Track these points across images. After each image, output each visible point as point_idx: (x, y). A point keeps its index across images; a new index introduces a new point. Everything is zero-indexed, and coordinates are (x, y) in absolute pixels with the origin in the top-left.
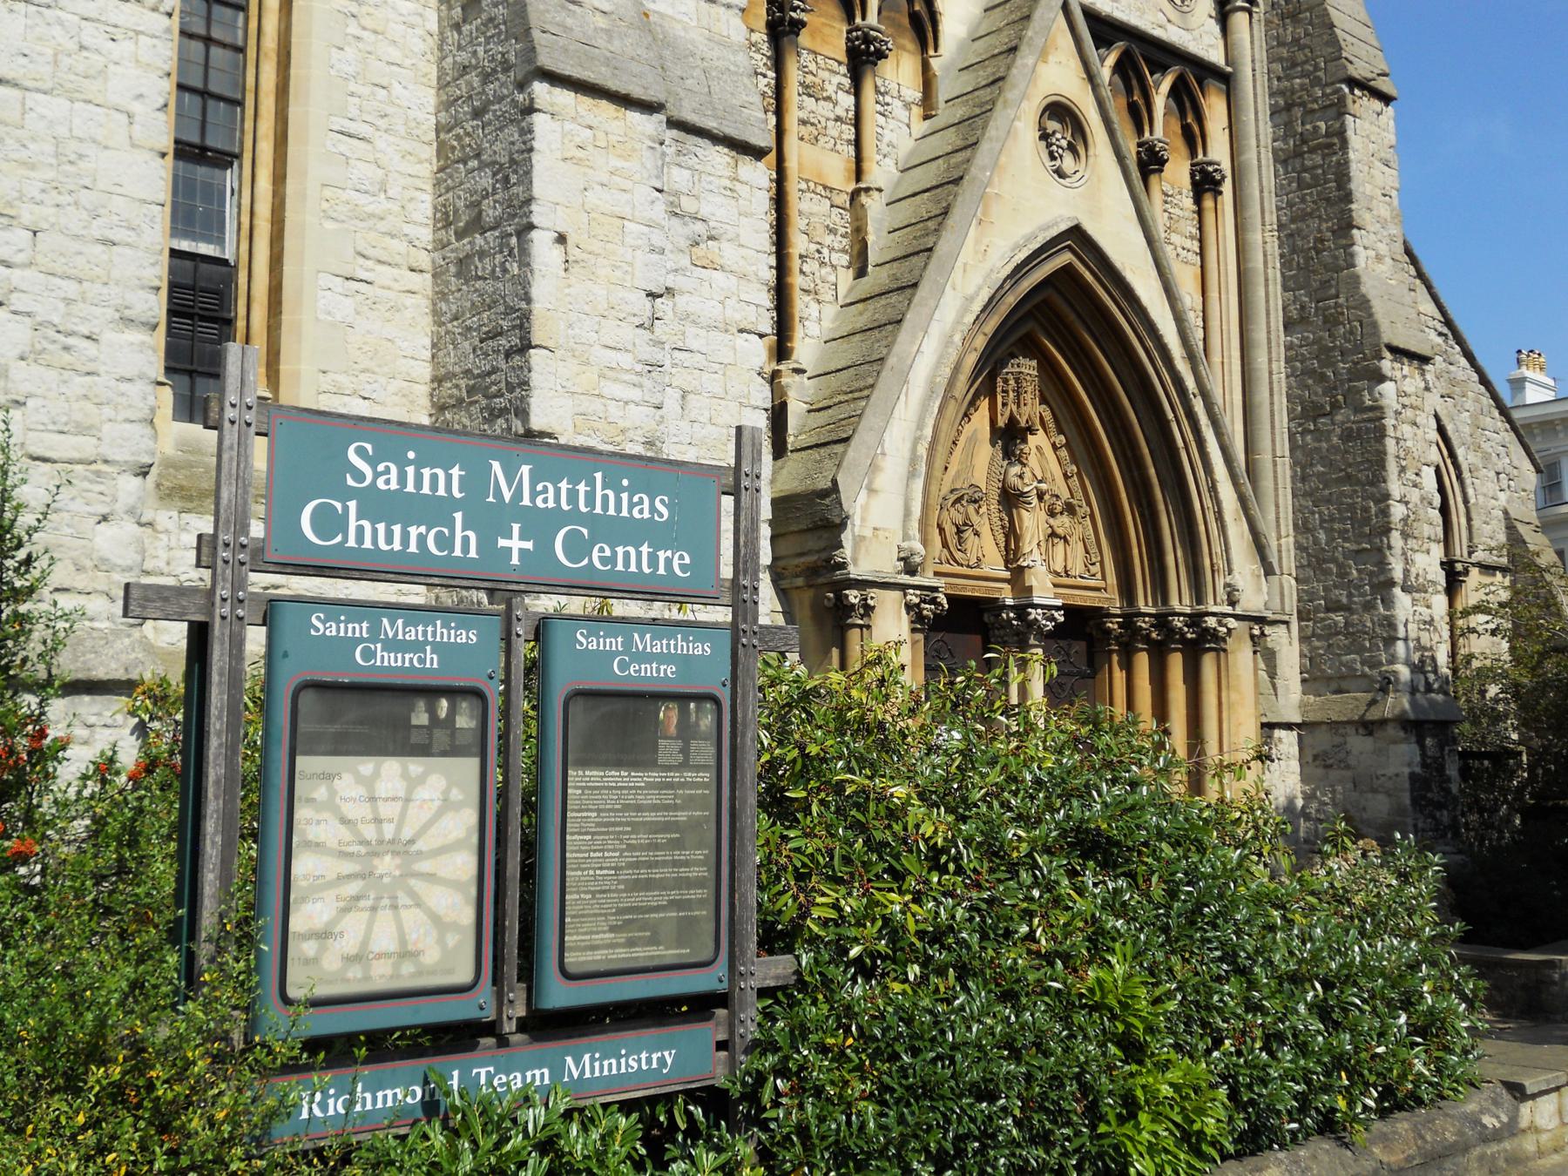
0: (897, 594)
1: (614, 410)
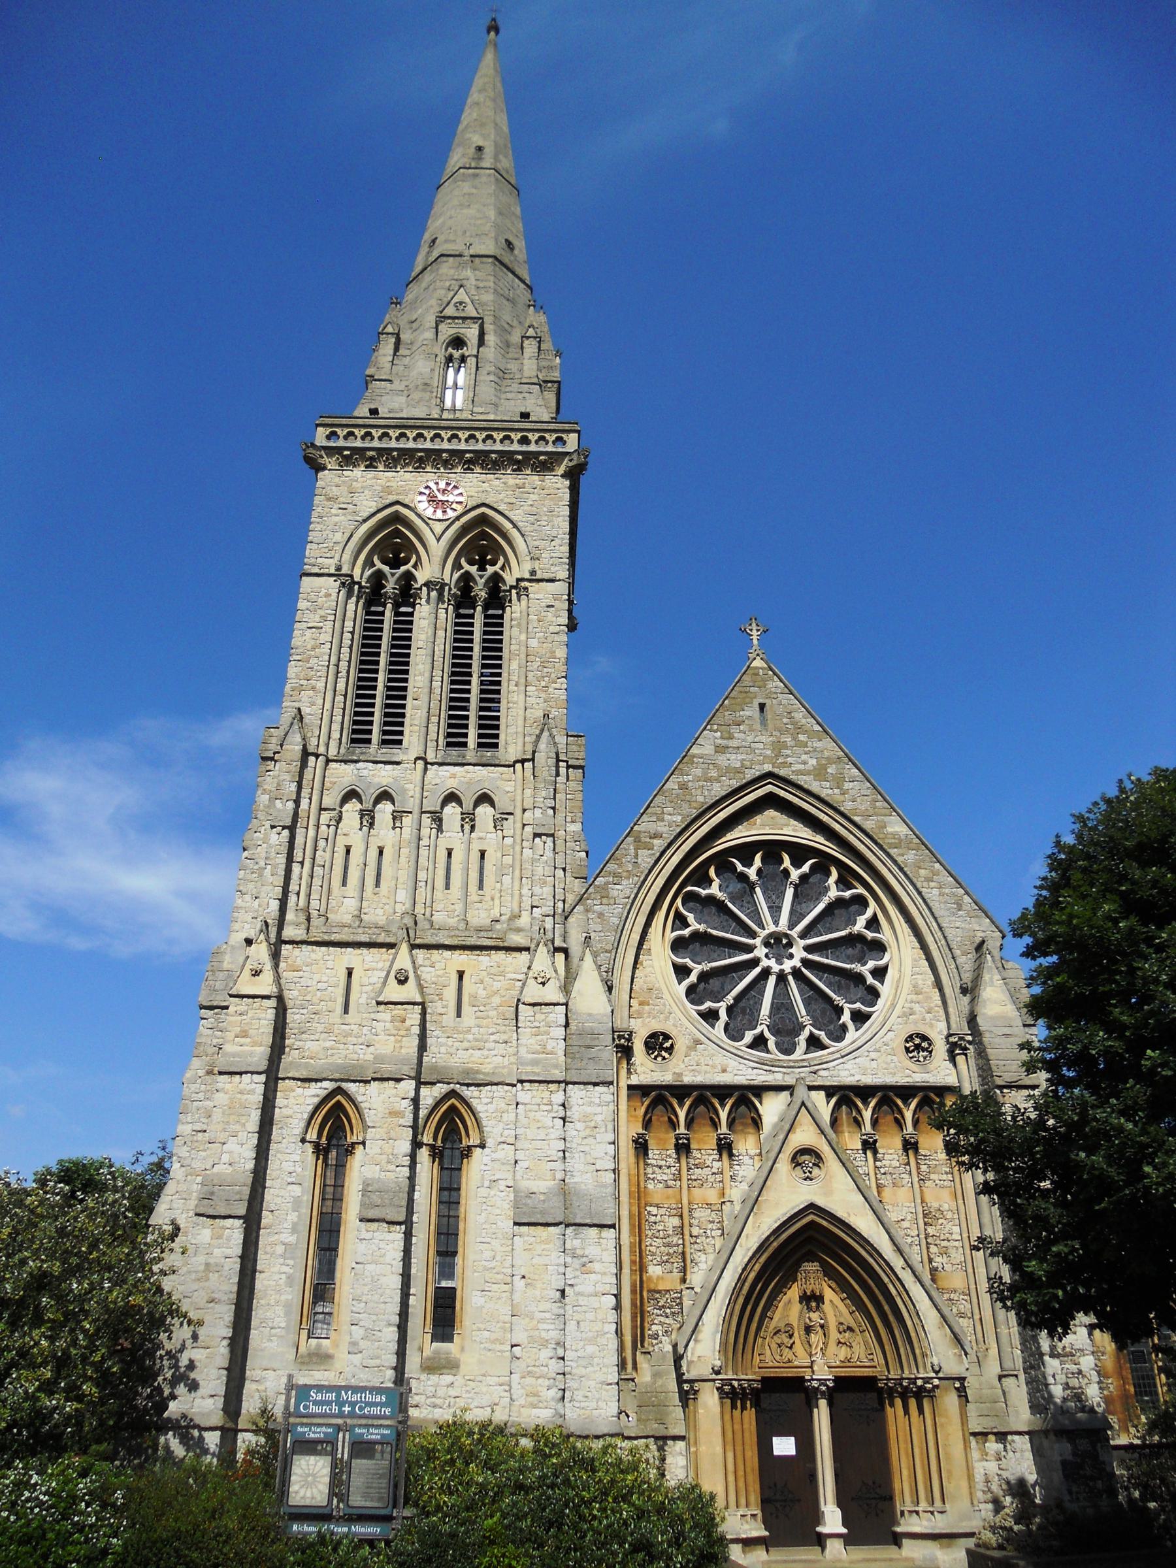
0: (711, 1383)
1: (544, 1334)
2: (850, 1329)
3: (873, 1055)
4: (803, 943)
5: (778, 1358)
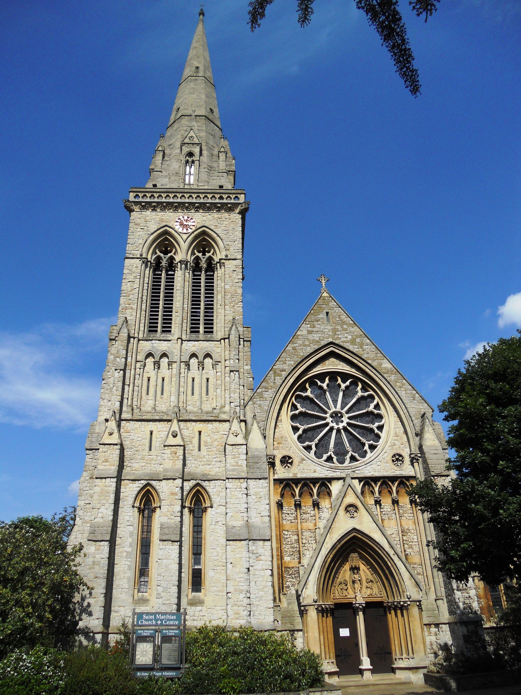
2: (371, 581)
3: (379, 463)
4: (347, 416)
5: (341, 595)
